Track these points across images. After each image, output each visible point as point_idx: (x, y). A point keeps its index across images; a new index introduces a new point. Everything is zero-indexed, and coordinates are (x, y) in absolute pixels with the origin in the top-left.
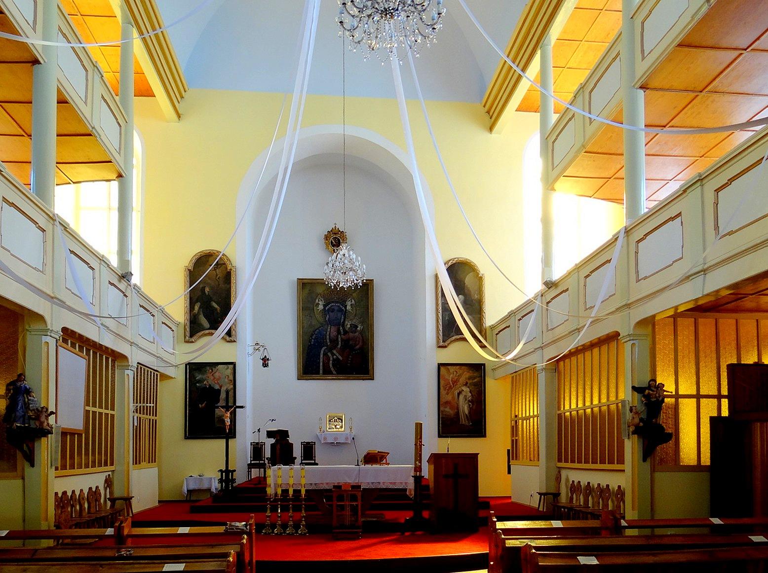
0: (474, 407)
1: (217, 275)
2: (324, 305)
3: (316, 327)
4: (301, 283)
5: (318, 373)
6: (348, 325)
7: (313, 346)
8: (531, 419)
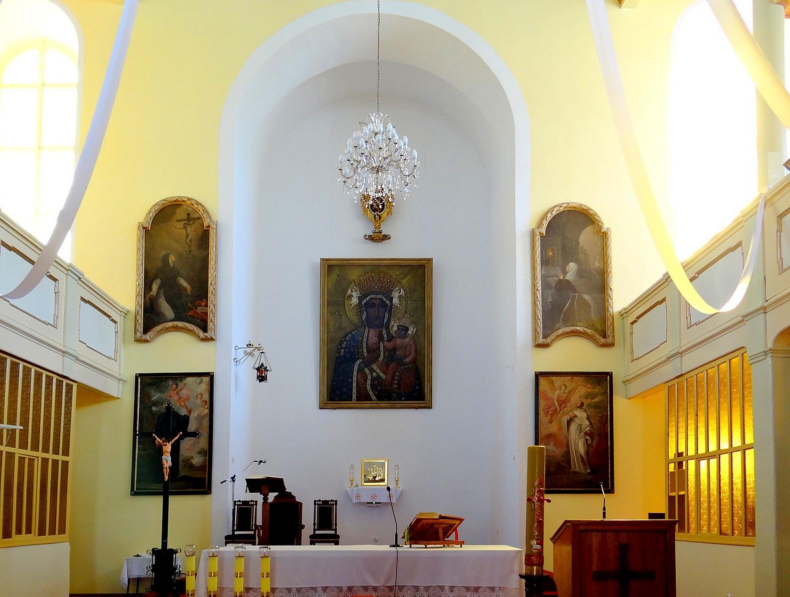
0: (594, 444)
1: (187, 236)
2: (359, 298)
3: (348, 330)
4: (327, 266)
5: (350, 399)
6: (394, 326)
7: (343, 359)
8: (725, 458)
